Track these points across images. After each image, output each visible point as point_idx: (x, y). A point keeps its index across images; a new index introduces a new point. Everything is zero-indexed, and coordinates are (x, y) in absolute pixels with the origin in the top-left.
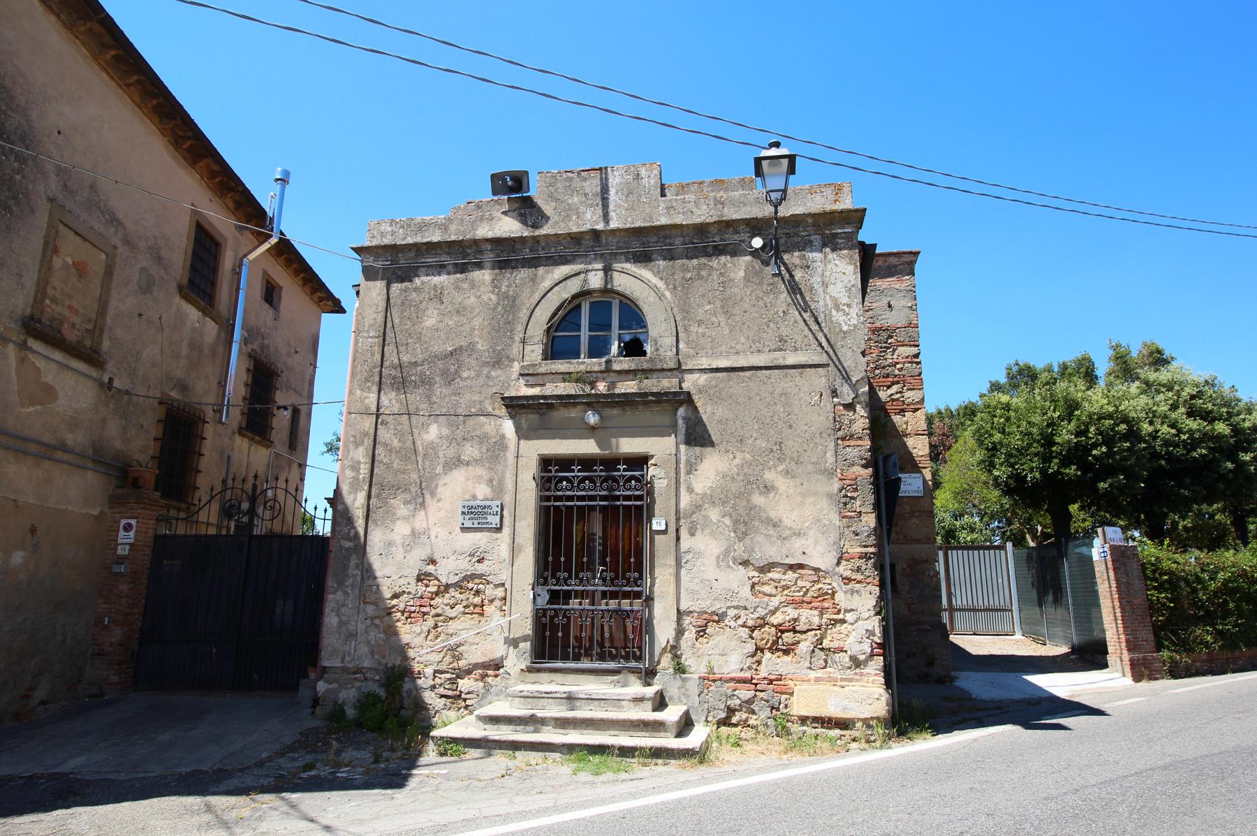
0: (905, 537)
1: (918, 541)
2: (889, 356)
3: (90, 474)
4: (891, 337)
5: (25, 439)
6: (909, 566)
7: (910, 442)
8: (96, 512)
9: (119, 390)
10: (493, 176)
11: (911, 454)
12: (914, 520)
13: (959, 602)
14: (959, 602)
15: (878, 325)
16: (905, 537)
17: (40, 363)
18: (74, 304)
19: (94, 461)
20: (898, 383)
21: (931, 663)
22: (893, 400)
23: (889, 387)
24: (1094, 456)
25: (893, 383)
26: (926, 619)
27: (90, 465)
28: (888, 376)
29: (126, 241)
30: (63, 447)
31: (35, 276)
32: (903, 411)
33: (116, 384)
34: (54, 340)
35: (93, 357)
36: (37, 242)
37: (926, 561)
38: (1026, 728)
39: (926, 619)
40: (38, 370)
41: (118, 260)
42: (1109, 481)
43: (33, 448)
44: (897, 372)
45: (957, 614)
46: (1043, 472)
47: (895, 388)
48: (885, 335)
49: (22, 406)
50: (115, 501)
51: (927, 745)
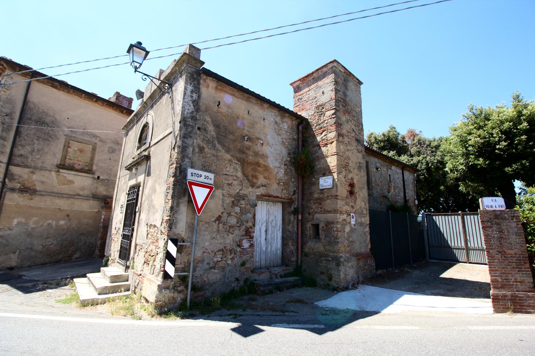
0: (324, 210)
1: (329, 212)
2: (322, 118)
3: (91, 201)
4: (323, 108)
5: (62, 194)
6: (326, 226)
7: (329, 160)
8: (96, 210)
9: (102, 179)
10: (143, 93)
11: (329, 166)
12: (329, 201)
13: (472, 245)
14: (472, 245)
15: (318, 104)
16: (324, 210)
17: (65, 175)
18: (79, 159)
19: (93, 198)
20: (325, 130)
21: (330, 279)
22: (323, 140)
23: (321, 134)
24: (499, 149)
25: (323, 131)
26: (331, 254)
27: (92, 199)
28: (321, 128)
29: (101, 141)
30: (79, 195)
31: (61, 155)
32: (326, 144)
33: (101, 178)
34: (71, 168)
35: (89, 171)
36: (61, 146)
37: (333, 223)
38: (320, 332)
39: (331, 254)
40: (66, 177)
41: (97, 146)
42: (514, 166)
43: (66, 196)
44: (325, 125)
45: (471, 252)
46: (467, 165)
47: (324, 134)
48: (321, 108)
49: (60, 186)
50: (102, 208)
51: (175, 323)
